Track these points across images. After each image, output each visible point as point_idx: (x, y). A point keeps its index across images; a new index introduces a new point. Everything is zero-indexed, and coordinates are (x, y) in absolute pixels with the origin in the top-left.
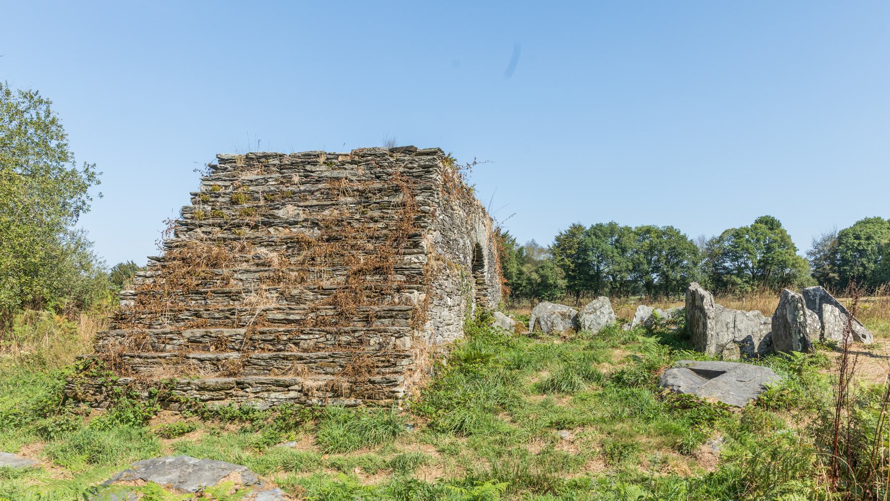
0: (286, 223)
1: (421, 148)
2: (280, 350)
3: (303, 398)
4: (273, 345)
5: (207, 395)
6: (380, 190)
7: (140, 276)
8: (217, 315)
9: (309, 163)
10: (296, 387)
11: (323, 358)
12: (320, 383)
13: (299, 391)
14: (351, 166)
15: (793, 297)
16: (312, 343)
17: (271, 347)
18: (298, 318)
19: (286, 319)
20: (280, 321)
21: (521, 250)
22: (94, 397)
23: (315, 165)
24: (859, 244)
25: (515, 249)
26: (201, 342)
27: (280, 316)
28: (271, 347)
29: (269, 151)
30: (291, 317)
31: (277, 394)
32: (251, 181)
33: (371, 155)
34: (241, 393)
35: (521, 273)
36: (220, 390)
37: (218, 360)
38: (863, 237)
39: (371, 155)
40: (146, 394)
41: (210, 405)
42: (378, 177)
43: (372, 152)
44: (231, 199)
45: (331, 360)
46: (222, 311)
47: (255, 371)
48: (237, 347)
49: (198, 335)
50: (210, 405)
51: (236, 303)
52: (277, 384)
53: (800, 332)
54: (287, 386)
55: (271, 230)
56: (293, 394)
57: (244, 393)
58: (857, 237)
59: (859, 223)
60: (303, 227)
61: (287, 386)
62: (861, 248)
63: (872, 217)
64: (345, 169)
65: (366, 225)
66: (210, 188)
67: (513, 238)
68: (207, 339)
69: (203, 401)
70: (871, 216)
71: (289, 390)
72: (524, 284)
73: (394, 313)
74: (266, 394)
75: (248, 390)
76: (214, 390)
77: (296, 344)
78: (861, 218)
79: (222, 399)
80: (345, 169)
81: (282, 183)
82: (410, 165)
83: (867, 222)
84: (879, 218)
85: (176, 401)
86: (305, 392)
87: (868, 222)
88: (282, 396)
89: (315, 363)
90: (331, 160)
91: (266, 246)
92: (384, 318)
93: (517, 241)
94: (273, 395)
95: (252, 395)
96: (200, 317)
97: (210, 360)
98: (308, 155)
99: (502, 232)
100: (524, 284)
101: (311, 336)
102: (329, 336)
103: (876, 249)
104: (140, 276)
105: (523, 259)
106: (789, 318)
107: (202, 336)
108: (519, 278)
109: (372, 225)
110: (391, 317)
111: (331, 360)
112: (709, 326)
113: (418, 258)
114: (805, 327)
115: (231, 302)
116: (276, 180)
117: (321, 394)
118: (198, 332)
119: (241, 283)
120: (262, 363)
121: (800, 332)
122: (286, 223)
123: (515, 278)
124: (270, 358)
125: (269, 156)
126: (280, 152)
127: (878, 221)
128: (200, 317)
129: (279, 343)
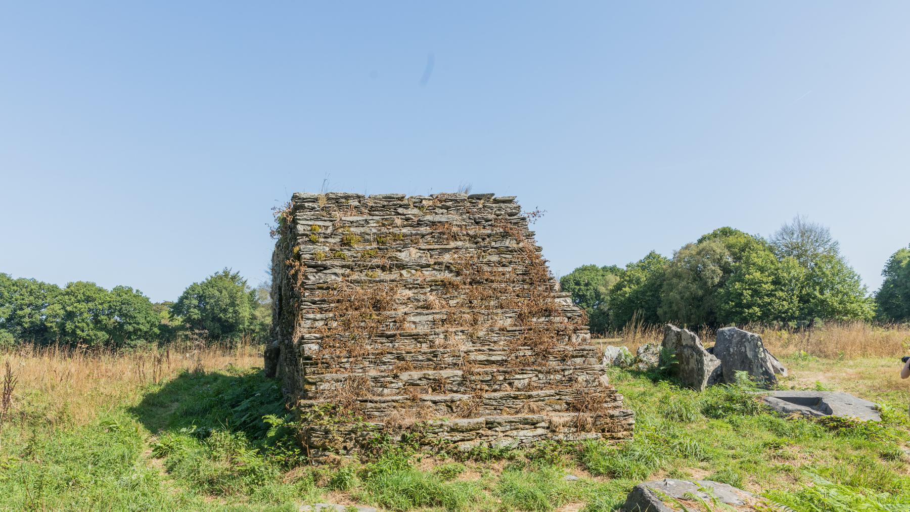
0: (418, 265)
1: (499, 196)
2: (495, 391)
3: (550, 435)
4: (489, 386)
5: (458, 436)
6: (489, 236)
7: (308, 319)
8: (420, 358)
9: (401, 206)
10: (543, 424)
11: (550, 396)
12: (566, 419)
13: (548, 428)
14: (441, 211)
15: (752, 336)
16: (526, 381)
17: (487, 388)
18: (499, 358)
19: (487, 361)
20: (481, 362)
21: (252, 294)
22: (344, 444)
23: (407, 208)
24: (579, 290)
25: (247, 291)
26: (418, 385)
27: (482, 357)
28: (487, 388)
29: (350, 192)
30: (493, 358)
31: (525, 431)
32: (352, 222)
33: (451, 200)
34: (489, 432)
35: (254, 318)
36: (471, 430)
37: (453, 401)
38: (582, 283)
39: (451, 200)
40: (399, 438)
41: (463, 446)
42: (477, 223)
43: (453, 198)
44: (342, 240)
45: (558, 397)
46: (425, 353)
47: (487, 411)
48: (455, 389)
49: (416, 377)
50: (463, 446)
51: (424, 345)
52: (525, 422)
53: (762, 366)
54: (534, 424)
55: (404, 272)
56: (540, 431)
57: (494, 433)
58: (578, 284)
59: (577, 270)
60: (434, 269)
61: (534, 424)
62: (581, 293)
63: (589, 265)
64: (436, 213)
65: (495, 269)
66: (309, 228)
67: (244, 280)
68: (424, 382)
69: (455, 442)
70: (588, 264)
71: (535, 428)
72: (257, 330)
73: (585, 352)
74: (515, 433)
75: (497, 429)
76: (468, 431)
77: (510, 384)
78: (579, 266)
79: (472, 440)
80: (436, 213)
81: (384, 225)
82: (498, 212)
83: (584, 269)
84: (594, 266)
85: (428, 444)
86: (552, 428)
87: (585, 270)
88: (530, 433)
89: (543, 401)
90: (418, 203)
91: (410, 289)
92: (577, 357)
93: (248, 283)
94: (522, 433)
95: (501, 434)
96: (403, 359)
97: (445, 401)
98: (389, 198)
99: (231, 273)
100: (257, 330)
101: (525, 376)
102: (540, 376)
103: (593, 294)
104: (308, 319)
105: (255, 303)
106: (750, 354)
107: (420, 379)
108: (251, 323)
109: (501, 269)
110: (582, 356)
111: (558, 397)
112: (705, 362)
113: (566, 301)
114: (766, 362)
115: (419, 345)
116: (378, 222)
117: (566, 430)
118: (416, 375)
119: (413, 326)
120: (494, 403)
121: (762, 366)
122: (418, 265)
123: (247, 323)
124: (501, 398)
125: (349, 197)
126: (360, 194)
127: (593, 268)
128: (403, 359)
129: (495, 383)
